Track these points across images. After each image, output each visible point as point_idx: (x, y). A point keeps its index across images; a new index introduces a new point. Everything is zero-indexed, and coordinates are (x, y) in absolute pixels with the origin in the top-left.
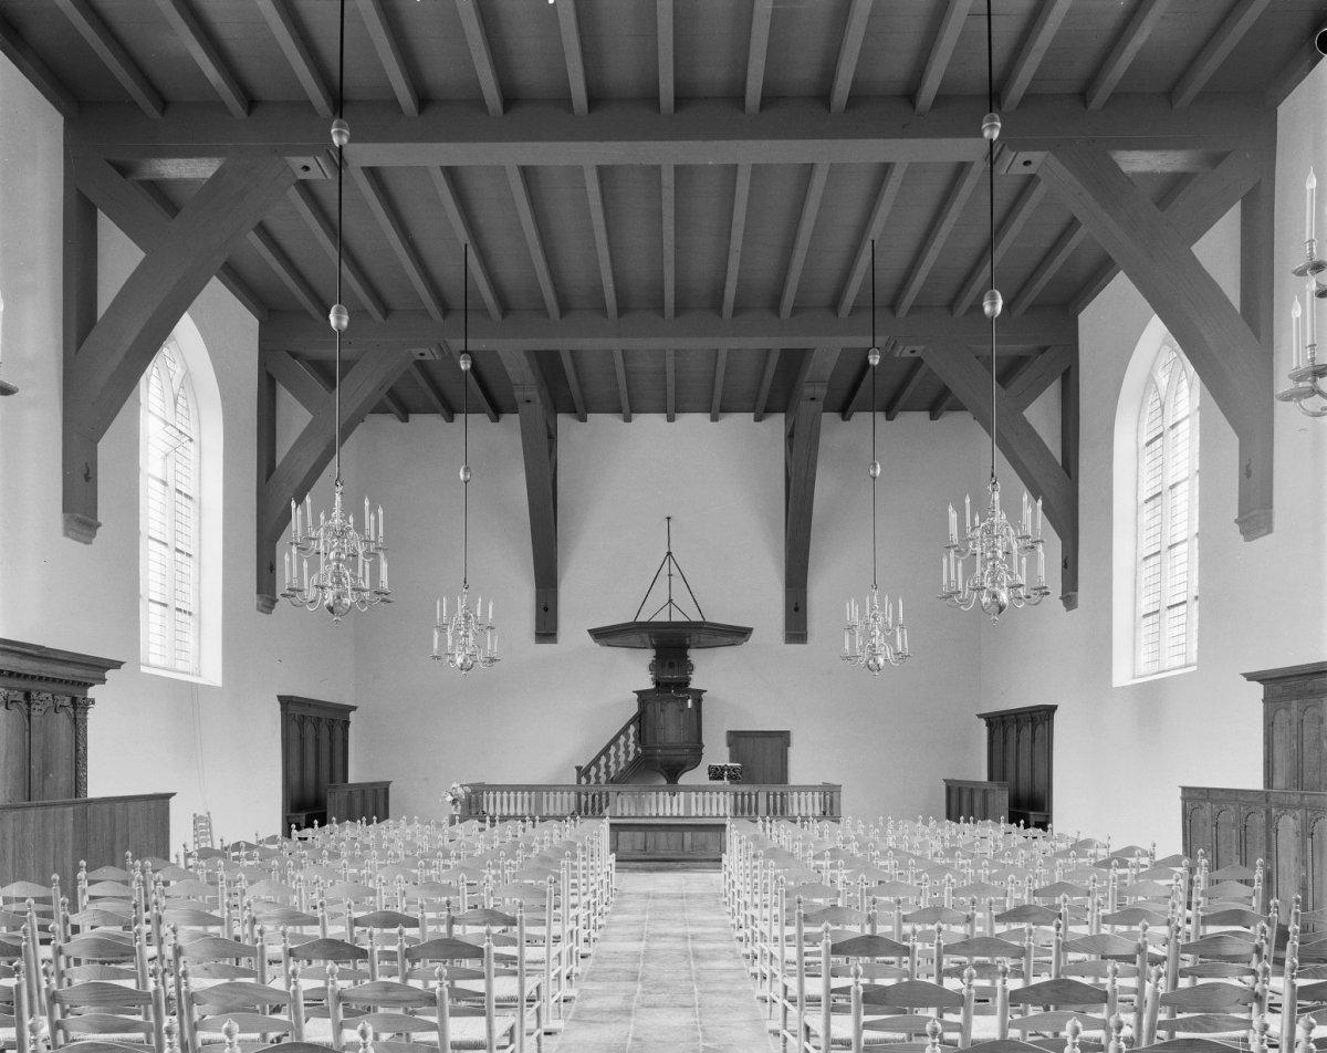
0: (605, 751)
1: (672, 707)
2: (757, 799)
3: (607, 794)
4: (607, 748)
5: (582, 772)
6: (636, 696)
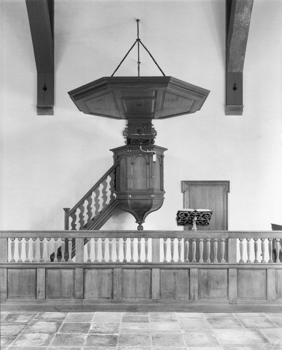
0: (88, 196)
1: (140, 161)
2: (74, 244)
3: (74, 241)
4: (89, 194)
5: (69, 213)
6: (112, 154)
